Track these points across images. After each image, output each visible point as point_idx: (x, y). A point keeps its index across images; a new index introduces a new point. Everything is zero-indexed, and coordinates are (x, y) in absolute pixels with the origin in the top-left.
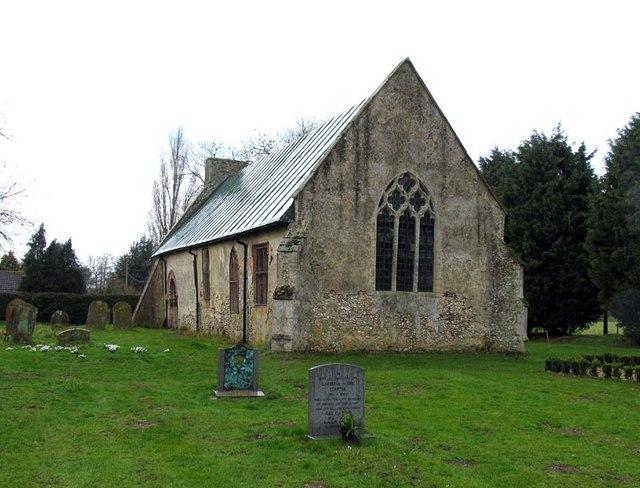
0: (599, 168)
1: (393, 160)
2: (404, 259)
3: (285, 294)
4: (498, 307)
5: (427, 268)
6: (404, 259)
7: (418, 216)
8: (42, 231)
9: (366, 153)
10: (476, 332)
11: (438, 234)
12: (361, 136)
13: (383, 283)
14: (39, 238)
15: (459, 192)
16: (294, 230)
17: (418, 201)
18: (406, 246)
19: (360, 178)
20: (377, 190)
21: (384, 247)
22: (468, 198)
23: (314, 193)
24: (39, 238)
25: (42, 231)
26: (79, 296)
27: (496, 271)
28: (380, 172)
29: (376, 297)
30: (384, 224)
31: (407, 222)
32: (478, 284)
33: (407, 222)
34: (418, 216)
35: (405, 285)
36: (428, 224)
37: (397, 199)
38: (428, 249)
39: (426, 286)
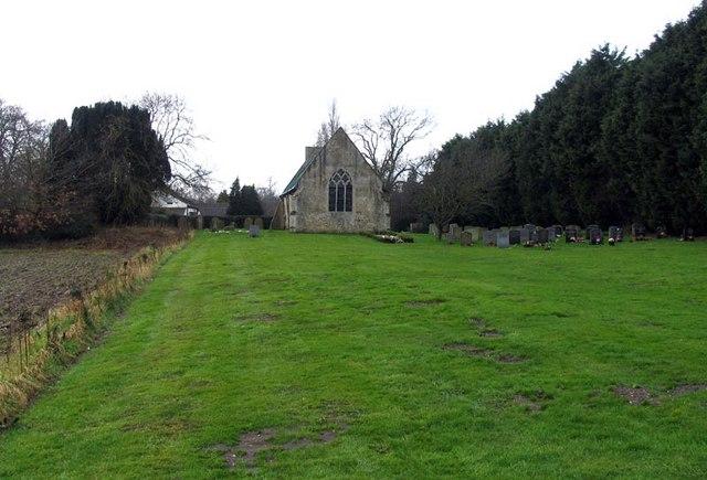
0: (69, 124)
1: (335, 165)
2: (341, 199)
3: (294, 213)
4: (378, 216)
5: (350, 202)
6: (341, 199)
7: (345, 184)
8: (237, 180)
9: (324, 163)
10: (370, 226)
11: (354, 190)
12: (316, 156)
13: (331, 209)
14: (236, 184)
15: (362, 174)
16: (298, 192)
17: (345, 179)
18: (340, 195)
19: (322, 172)
20: (329, 176)
21: (332, 196)
22: (367, 176)
23: (558, 109)
24: (236, 184)
25: (237, 180)
26: (606, 76)
27: (378, 204)
28: (330, 169)
29: (329, 214)
30: (332, 189)
31: (341, 189)
32: (370, 208)
33: (341, 189)
34: (345, 184)
35: (340, 209)
36: (350, 188)
37: (336, 178)
38: (350, 196)
39: (349, 209)
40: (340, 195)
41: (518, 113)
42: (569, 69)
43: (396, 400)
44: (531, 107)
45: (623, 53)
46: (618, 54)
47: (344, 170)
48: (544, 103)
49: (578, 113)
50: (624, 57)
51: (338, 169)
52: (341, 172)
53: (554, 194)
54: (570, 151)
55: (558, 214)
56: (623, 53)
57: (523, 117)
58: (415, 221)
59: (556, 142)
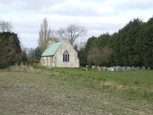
3: (54, 62)
5: (68, 59)
8: (45, 21)
18: (66, 57)
21: (64, 57)
25: (45, 21)
30: (64, 55)
33: (66, 55)
34: (67, 54)
35: (66, 61)
36: (69, 55)
37: (65, 53)
38: (69, 58)
39: (68, 61)
40: (66, 57)
41: (114, 33)
42: (128, 23)
43: (133, 58)
44: (117, 32)
45: (142, 20)
46: (141, 20)
47: (67, 50)
48: (120, 31)
49: (130, 37)
50: (142, 22)
51: (66, 50)
52: (66, 51)
53: (123, 58)
54: (128, 47)
55: (125, 63)
56: (142, 20)
57: (115, 34)
58: (88, 65)
59: (124, 44)
